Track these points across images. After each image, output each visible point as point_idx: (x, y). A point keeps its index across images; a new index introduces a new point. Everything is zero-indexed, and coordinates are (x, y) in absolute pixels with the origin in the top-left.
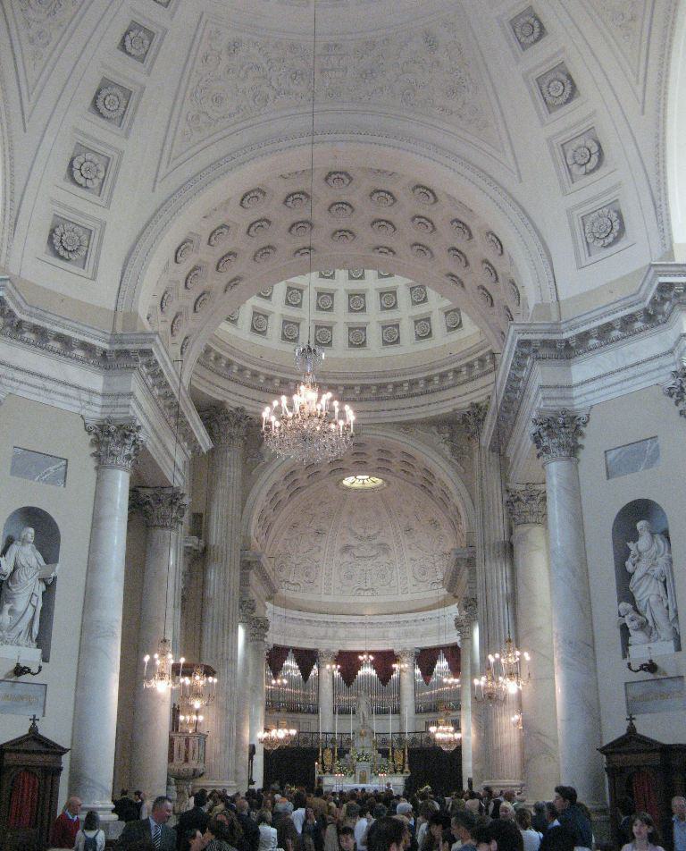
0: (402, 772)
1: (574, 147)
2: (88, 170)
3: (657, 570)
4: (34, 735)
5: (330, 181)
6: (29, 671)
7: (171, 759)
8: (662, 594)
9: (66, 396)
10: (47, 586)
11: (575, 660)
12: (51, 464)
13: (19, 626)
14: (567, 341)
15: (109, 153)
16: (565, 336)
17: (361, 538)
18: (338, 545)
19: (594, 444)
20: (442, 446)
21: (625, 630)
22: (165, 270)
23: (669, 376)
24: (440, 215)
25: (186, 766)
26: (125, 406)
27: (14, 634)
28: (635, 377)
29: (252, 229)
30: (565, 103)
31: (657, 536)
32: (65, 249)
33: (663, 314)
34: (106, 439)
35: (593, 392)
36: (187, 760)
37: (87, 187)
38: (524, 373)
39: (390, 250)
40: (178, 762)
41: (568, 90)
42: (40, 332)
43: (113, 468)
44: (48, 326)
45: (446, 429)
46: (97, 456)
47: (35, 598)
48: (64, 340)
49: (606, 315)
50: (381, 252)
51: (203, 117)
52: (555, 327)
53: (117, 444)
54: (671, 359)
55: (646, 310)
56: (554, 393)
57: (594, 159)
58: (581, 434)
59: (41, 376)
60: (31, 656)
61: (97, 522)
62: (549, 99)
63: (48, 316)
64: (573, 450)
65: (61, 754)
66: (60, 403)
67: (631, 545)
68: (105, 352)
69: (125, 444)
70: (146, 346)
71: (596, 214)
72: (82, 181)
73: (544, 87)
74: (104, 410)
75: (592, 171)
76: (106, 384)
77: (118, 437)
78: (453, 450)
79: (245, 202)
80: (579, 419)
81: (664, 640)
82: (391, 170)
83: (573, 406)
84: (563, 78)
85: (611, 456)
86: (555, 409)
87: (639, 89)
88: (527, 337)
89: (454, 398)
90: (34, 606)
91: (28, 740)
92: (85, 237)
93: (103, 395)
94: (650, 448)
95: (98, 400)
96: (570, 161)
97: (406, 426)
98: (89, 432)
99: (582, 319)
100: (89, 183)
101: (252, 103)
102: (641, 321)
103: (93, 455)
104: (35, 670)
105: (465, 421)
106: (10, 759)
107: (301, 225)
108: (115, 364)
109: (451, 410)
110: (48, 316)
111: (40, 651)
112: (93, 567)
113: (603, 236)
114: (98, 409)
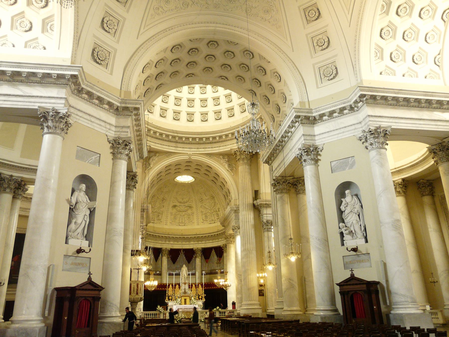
0: (201, 299)
1: (318, 38)
2: (110, 24)
3: (356, 210)
4: (90, 282)
5: (209, 45)
6: (84, 251)
7: (130, 294)
8: (358, 220)
9: (100, 125)
10: (91, 212)
11: (321, 246)
12: (93, 156)
13: (78, 230)
14: (315, 117)
15: (120, 18)
16: (314, 115)
17: (180, 202)
18: (172, 204)
19: (325, 158)
20: (224, 164)
21: (342, 234)
22: (139, 76)
23: (361, 132)
24: (253, 63)
25: (137, 296)
26: (126, 132)
27: (76, 233)
28: (343, 132)
29: (173, 62)
30: (315, 20)
31: (354, 196)
32: (99, 59)
33: (358, 107)
34: (118, 146)
35: (325, 138)
36: (137, 294)
37: (109, 32)
38: (293, 130)
39: (226, 78)
40: (133, 294)
41: (317, 14)
42: (90, 94)
43: (120, 159)
44: (94, 92)
45: (226, 157)
46: (113, 154)
47: (86, 216)
48: (100, 99)
49: (332, 107)
50: (222, 78)
51: (160, 9)
52: (310, 111)
53: (123, 149)
54: (359, 126)
55: (351, 106)
56: (308, 138)
57: (326, 44)
58: (320, 155)
59: (89, 115)
60: (85, 244)
61: (113, 184)
62: (308, 18)
63: (95, 87)
64: (316, 161)
65: (101, 290)
66: (97, 128)
67: (343, 199)
68: (118, 107)
69: (126, 149)
70: (137, 106)
71: (326, 66)
72: (107, 29)
73: (307, 14)
74: (116, 133)
75: (324, 49)
76: (116, 121)
77: (123, 146)
78: (229, 165)
79: (173, 50)
80: (319, 149)
81: (360, 238)
82: (237, 42)
83: (316, 143)
84: (316, 10)
85: (333, 164)
86: (309, 144)
87: (349, 17)
88: (299, 114)
89: (233, 144)
90: (85, 221)
91: (87, 284)
92: (107, 55)
93: (116, 127)
94: (351, 161)
95: (114, 129)
96: (315, 44)
97: (210, 155)
98: (110, 143)
99: (322, 108)
100: (110, 30)
101: (182, 6)
102: (348, 110)
103: (111, 153)
104: (87, 250)
105: (235, 154)
106: (79, 293)
107: (192, 63)
108: (121, 113)
109: (229, 149)
110: (95, 87)
111: (87, 242)
112: (111, 203)
113: (329, 75)
114: (113, 133)
